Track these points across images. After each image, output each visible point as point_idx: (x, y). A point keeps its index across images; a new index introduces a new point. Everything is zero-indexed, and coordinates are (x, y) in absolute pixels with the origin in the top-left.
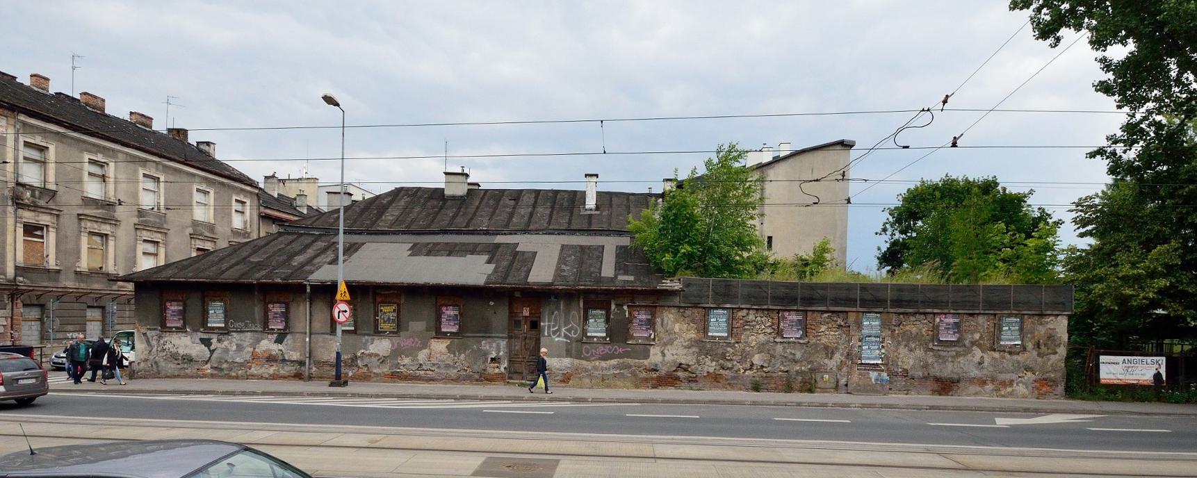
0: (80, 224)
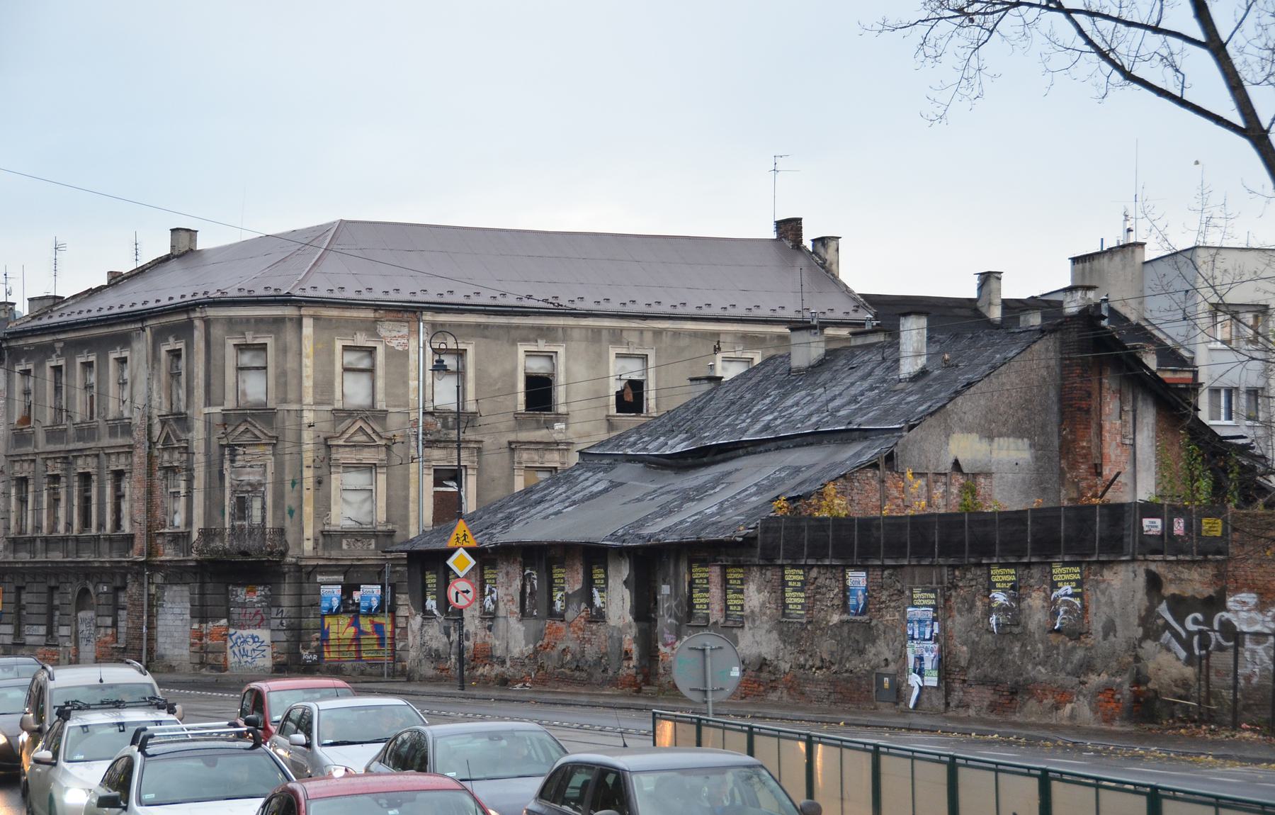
0: (512, 457)
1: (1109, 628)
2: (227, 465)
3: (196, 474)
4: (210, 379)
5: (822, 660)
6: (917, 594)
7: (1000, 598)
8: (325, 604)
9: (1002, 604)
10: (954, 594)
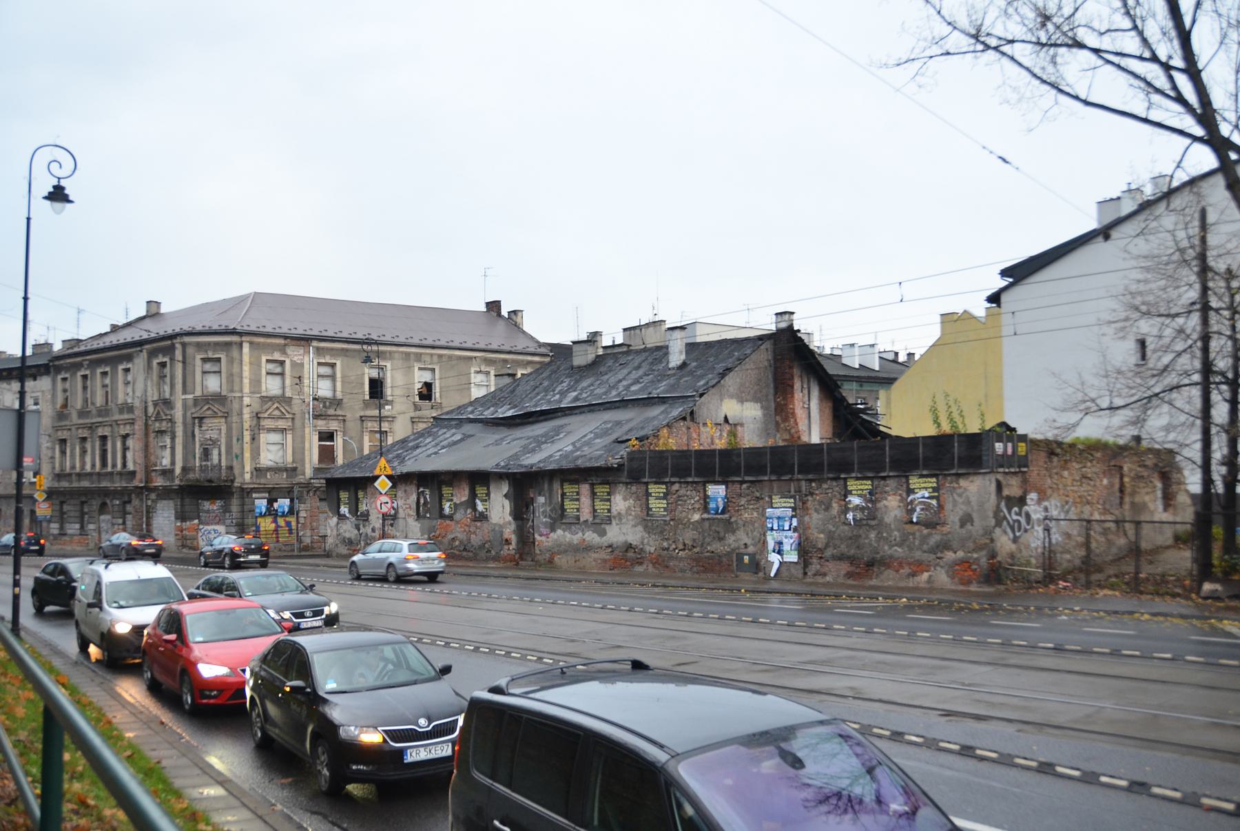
1: (966, 520)
3: (177, 434)
5: (685, 545)
6: (776, 499)
7: (855, 501)
8: (258, 511)
9: (858, 505)
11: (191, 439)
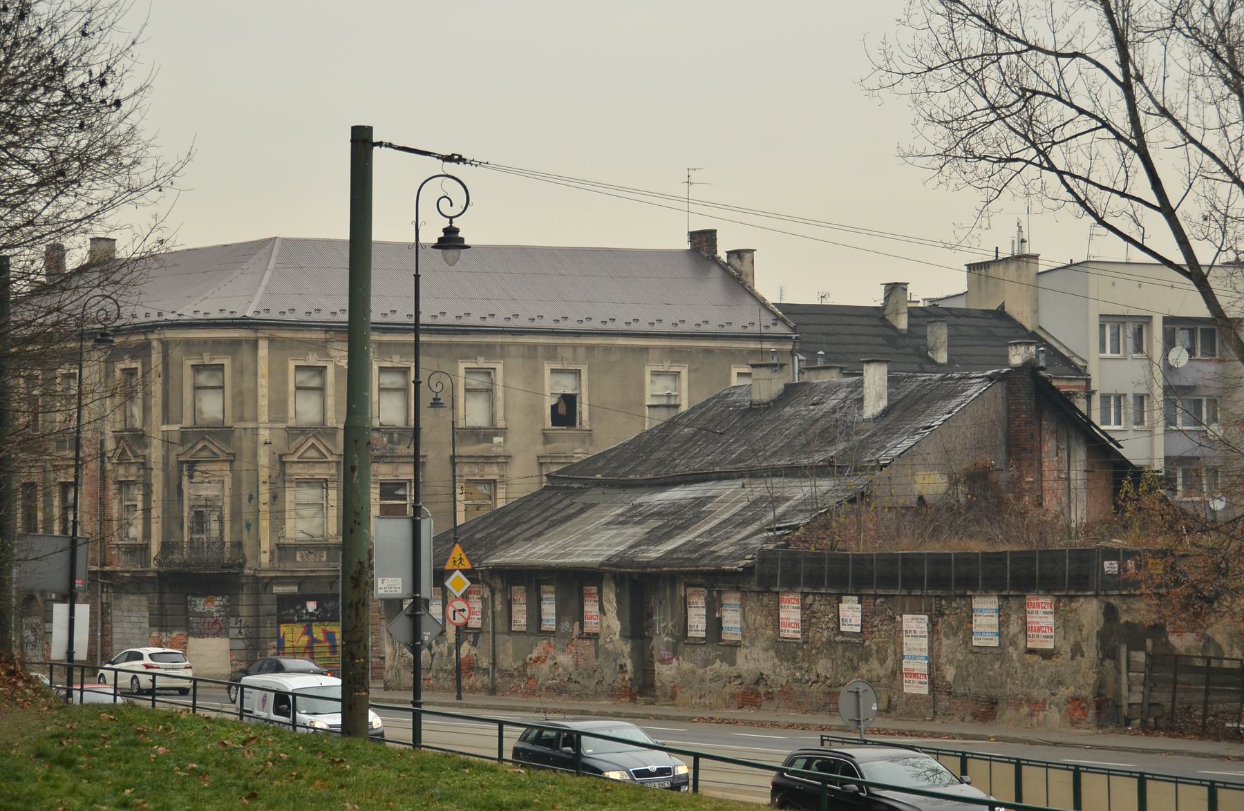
2: (185, 480)
3: (154, 488)
4: (168, 397)
10: (940, 620)
11: (176, 497)
